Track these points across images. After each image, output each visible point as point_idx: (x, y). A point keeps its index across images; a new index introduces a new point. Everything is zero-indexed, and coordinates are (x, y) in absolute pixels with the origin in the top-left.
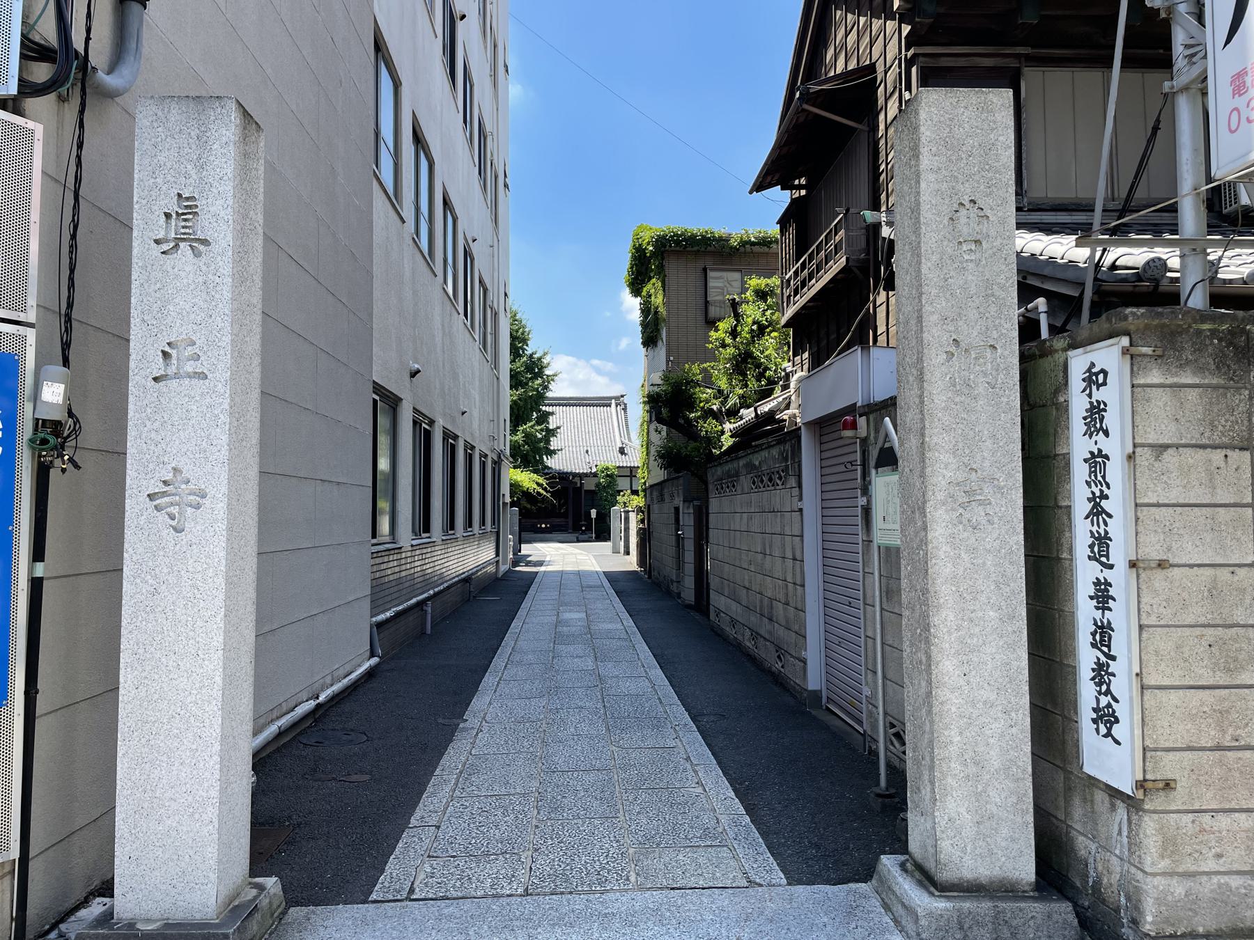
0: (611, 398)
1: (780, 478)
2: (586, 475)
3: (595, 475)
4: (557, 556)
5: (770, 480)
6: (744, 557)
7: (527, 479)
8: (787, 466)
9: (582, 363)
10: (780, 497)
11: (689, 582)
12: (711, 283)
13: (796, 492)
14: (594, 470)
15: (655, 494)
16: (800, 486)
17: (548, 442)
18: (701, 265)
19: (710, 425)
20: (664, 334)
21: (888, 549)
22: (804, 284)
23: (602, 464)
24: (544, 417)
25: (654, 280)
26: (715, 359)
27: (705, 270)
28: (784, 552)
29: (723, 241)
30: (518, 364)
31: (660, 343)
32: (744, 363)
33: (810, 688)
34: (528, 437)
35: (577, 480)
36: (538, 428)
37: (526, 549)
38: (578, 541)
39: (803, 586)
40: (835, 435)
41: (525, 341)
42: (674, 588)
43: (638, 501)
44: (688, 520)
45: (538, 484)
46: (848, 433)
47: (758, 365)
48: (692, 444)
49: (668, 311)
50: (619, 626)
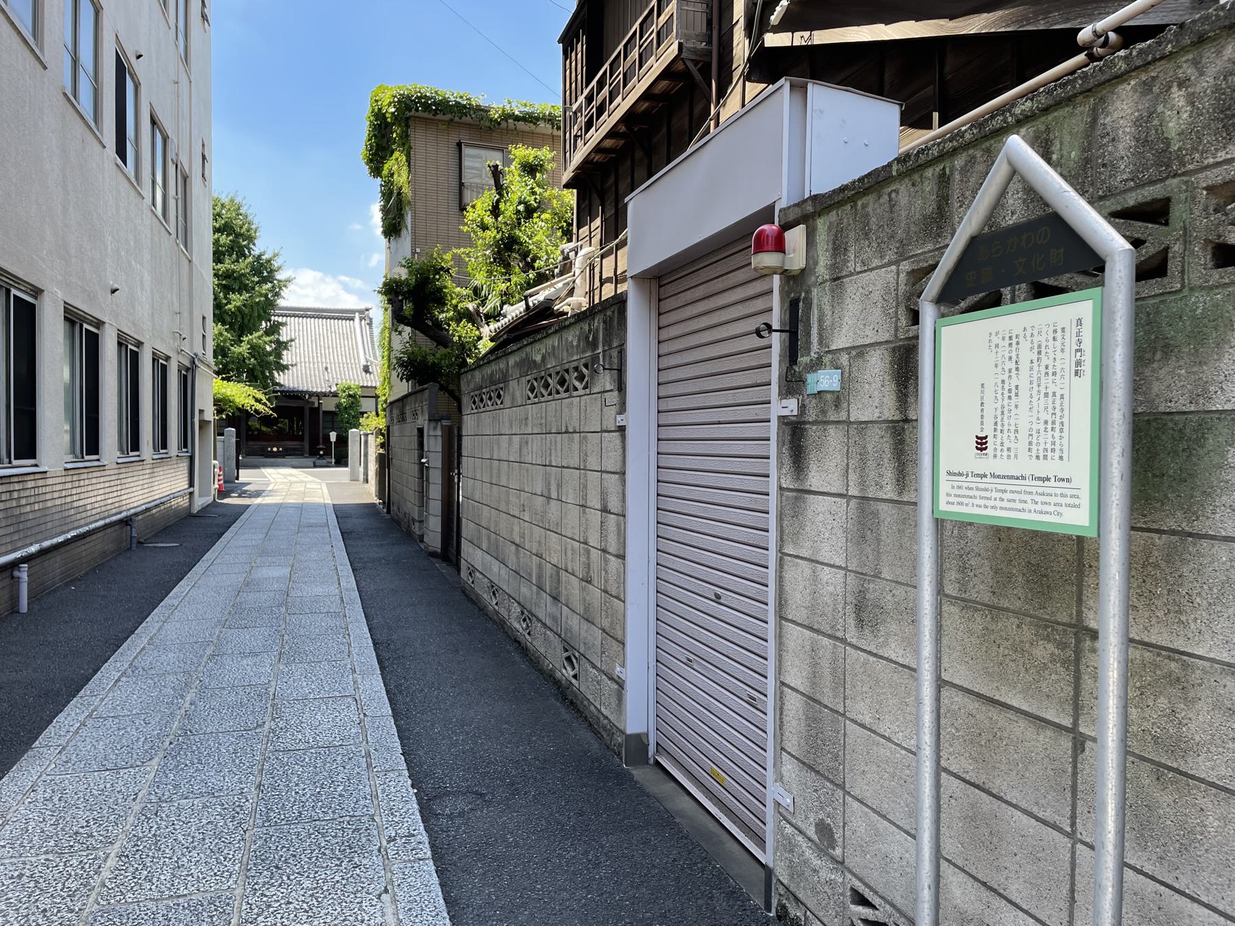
0: (353, 312)
1: (581, 378)
2: (325, 395)
3: (335, 395)
4: (286, 485)
5: (562, 382)
6: (513, 499)
7: (242, 394)
8: (595, 359)
9: (329, 279)
10: (579, 408)
11: (434, 524)
12: (467, 162)
13: (613, 397)
14: (334, 389)
15: (396, 412)
16: (621, 387)
17: (279, 356)
18: (454, 139)
19: (463, 331)
20: (409, 219)
21: (1007, 540)
22: (601, 110)
23: (344, 383)
24: (274, 329)
25: (396, 154)
26: (471, 244)
27: (459, 145)
28: (585, 497)
29: (481, 111)
30: (242, 265)
31: (404, 232)
32: (509, 251)
33: (629, 732)
34: (255, 349)
35: (314, 399)
36: (268, 339)
37: (245, 475)
38: (315, 466)
39: (622, 557)
40: (738, 260)
41: (251, 239)
42: (416, 528)
43: (381, 423)
44: (434, 445)
45: (258, 400)
46: (768, 259)
47: (525, 255)
48: (442, 351)
49: (414, 192)
50: (334, 590)
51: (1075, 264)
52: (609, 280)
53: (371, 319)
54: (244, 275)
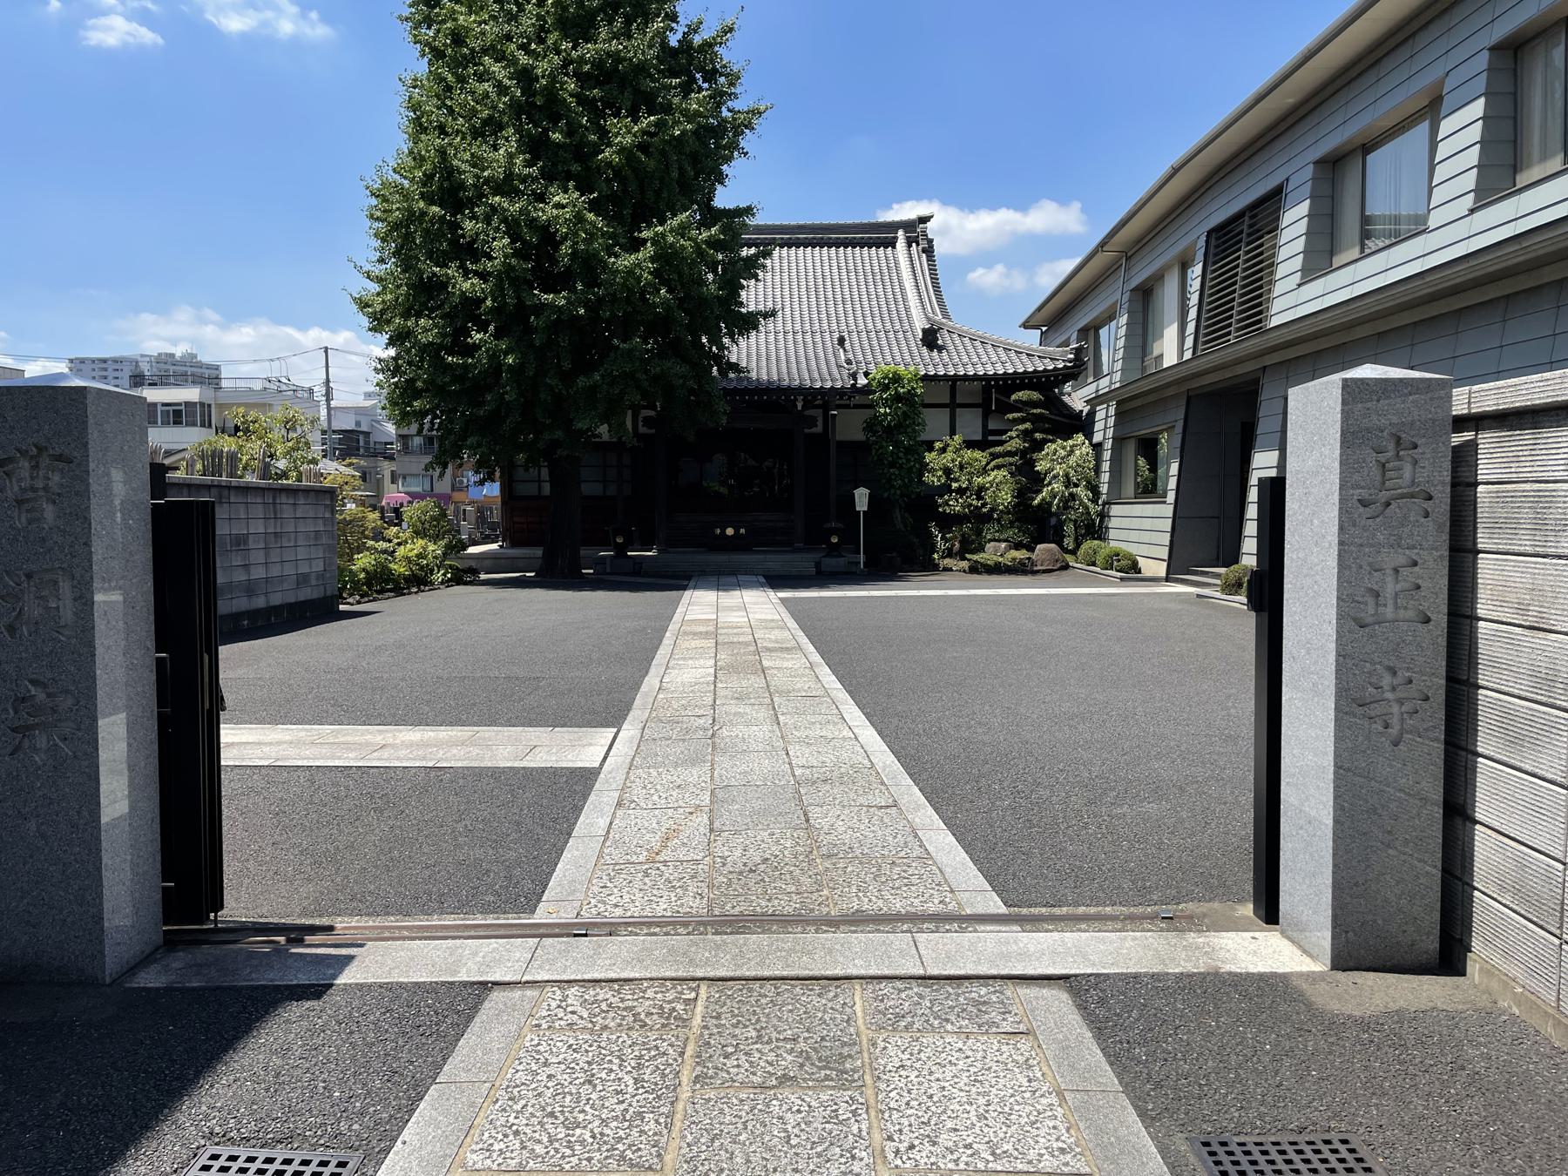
0: (893, 227)
14: (862, 381)
17: (732, 288)
34: (666, 258)
51: (1472, 446)
54: (641, 69)
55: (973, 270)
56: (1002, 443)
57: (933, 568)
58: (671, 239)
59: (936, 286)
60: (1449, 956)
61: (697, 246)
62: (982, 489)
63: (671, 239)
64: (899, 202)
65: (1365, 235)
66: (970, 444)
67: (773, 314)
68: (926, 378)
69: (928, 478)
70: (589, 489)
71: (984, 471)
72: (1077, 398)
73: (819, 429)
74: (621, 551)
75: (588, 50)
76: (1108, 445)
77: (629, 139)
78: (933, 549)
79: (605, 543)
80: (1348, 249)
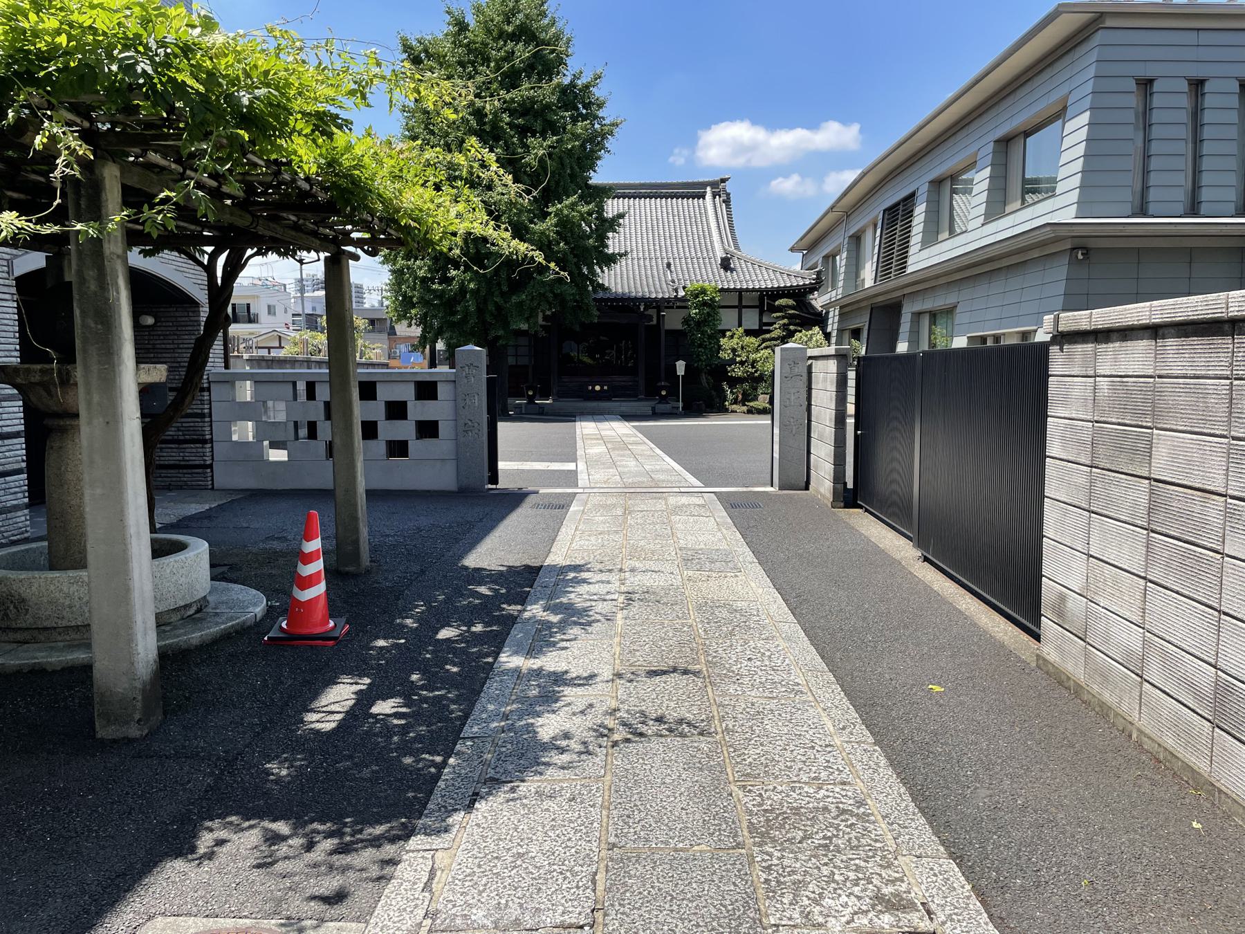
0: (704, 185)
14: (682, 293)
17: (602, 239)
52: (184, 172)
53: (728, 195)
54: (548, 107)
55: (776, 178)
56: (769, 332)
57: (722, 410)
58: (566, 212)
59: (731, 226)
60: (807, 488)
61: (582, 215)
62: (755, 361)
63: (566, 212)
64: (716, 123)
65: (1025, 191)
66: (748, 333)
67: (626, 254)
68: (722, 290)
69: (722, 354)
70: (511, 361)
71: (757, 350)
72: (818, 301)
73: (655, 322)
74: (531, 400)
75: (514, 94)
76: (834, 334)
77: (541, 152)
78: (725, 399)
79: (520, 395)
80: (1012, 202)
